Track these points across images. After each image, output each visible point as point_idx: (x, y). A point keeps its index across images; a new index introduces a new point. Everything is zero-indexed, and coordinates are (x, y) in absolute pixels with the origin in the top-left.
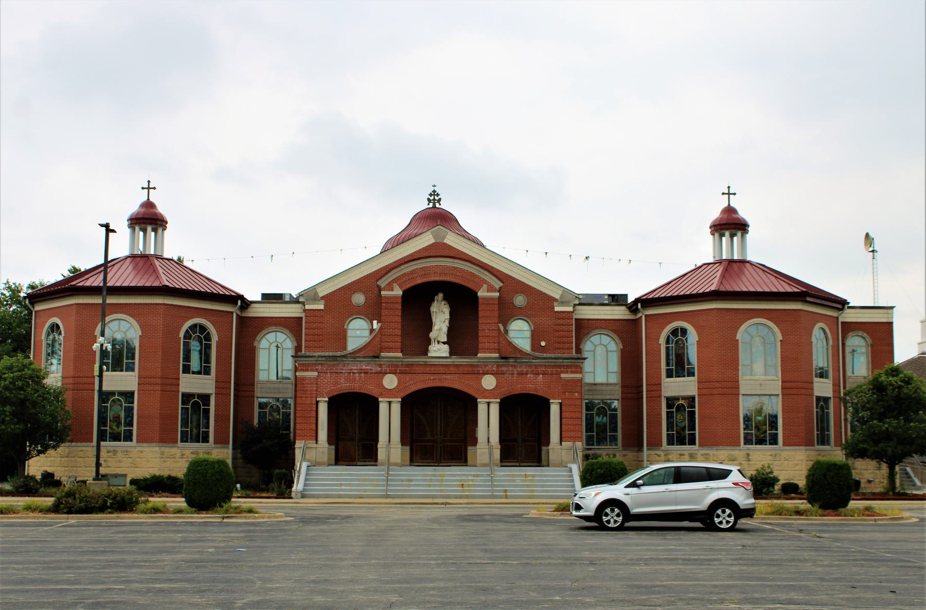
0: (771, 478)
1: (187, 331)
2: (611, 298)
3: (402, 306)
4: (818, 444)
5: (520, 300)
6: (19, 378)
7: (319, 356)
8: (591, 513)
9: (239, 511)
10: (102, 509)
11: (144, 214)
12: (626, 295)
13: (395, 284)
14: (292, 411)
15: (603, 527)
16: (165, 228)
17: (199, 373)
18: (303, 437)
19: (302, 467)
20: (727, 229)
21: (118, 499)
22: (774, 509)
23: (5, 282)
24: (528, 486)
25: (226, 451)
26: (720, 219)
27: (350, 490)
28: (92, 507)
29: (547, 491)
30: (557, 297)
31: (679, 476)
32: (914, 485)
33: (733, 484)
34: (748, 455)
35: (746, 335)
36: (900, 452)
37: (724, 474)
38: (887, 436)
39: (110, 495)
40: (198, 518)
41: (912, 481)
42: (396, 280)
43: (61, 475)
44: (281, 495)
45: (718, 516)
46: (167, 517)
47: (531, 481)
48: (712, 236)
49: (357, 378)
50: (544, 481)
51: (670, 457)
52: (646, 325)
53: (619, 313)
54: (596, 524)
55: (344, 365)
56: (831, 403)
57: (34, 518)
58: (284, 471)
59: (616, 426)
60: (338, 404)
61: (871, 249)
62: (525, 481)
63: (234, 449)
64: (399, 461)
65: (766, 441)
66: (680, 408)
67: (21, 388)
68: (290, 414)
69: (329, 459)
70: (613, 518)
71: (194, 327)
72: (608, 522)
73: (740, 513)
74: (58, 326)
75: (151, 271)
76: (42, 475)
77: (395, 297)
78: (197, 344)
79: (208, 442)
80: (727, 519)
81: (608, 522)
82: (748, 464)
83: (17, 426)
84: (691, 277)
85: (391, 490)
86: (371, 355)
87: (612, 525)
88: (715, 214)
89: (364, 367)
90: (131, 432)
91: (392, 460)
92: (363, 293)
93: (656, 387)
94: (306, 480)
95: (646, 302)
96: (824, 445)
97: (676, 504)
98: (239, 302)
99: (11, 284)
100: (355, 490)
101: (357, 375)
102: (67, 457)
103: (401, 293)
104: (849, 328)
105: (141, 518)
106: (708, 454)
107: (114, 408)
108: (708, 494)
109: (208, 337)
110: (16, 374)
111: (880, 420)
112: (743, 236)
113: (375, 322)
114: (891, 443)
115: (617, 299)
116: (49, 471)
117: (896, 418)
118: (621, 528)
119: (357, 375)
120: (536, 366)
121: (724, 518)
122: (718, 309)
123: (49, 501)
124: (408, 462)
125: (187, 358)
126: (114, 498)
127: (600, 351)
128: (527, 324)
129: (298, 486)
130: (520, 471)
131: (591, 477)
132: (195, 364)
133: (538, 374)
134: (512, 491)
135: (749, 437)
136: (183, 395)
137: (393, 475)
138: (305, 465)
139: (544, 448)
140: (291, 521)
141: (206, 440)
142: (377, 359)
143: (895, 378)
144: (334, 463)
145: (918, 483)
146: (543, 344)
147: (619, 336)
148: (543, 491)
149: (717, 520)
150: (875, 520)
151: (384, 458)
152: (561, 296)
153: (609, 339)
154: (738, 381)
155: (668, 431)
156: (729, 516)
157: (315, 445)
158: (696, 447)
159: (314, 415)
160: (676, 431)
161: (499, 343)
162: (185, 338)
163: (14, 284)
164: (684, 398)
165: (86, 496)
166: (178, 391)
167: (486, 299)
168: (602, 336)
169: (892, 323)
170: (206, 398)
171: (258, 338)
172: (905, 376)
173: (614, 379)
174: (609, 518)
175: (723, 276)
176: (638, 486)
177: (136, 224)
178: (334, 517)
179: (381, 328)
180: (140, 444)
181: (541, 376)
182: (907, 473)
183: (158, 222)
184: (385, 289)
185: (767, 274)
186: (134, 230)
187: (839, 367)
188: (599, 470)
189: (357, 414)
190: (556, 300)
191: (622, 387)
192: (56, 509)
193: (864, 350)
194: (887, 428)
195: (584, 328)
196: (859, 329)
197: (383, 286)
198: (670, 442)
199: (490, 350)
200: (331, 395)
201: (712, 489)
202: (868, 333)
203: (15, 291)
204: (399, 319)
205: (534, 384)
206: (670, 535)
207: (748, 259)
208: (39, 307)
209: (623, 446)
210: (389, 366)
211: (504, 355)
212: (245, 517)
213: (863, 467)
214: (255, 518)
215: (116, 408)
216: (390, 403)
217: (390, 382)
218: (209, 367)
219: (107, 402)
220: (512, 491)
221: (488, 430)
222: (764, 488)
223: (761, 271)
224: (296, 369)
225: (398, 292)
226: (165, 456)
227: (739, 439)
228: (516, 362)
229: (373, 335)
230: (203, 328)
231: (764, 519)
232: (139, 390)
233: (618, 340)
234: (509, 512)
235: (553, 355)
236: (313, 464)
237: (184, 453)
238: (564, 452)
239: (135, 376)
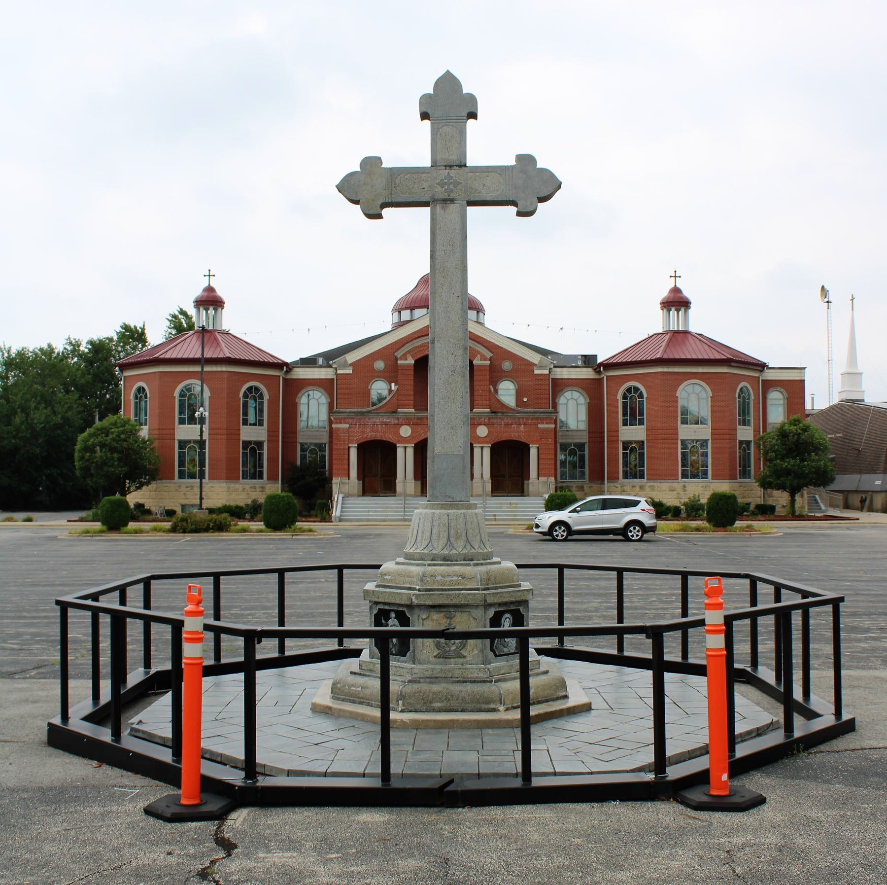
0: (698, 504)
1: (245, 392)
2: (583, 358)
3: (414, 377)
4: (740, 478)
5: (507, 365)
6: (123, 433)
7: (350, 412)
8: (546, 530)
9: (303, 531)
10: (207, 530)
11: (207, 297)
12: (596, 356)
14: (327, 453)
15: (554, 540)
16: (223, 308)
17: (255, 424)
18: (339, 475)
19: (337, 497)
20: (673, 306)
21: (217, 523)
22: (681, 527)
23: (67, 338)
24: (512, 512)
25: (276, 485)
26: (668, 297)
27: (376, 516)
28: (200, 529)
29: (527, 515)
30: (537, 362)
31: (606, 505)
32: (820, 509)
33: (642, 510)
34: (685, 486)
35: (684, 393)
36: (796, 484)
37: (635, 504)
38: (788, 472)
40: (275, 535)
41: (819, 506)
42: (408, 352)
43: (151, 505)
44: (323, 520)
45: (631, 531)
46: (253, 535)
47: (515, 507)
48: (661, 311)
49: (380, 429)
50: (524, 508)
51: (625, 488)
52: (607, 384)
53: (587, 373)
54: (550, 538)
55: (369, 419)
56: (752, 445)
57: (161, 536)
58: (324, 501)
59: (584, 464)
60: (365, 449)
61: (826, 300)
62: (510, 508)
63: (283, 483)
64: (413, 493)
65: (699, 476)
66: (633, 450)
67: (125, 440)
68: (325, 456)
69: (358, 491)
70: (560, 533)
71: (250, 389)
72: (557, 536)
73: (645, 529)
74: (144, 389)
75: (215, 344)
76: (134, 504)
77: (409, 365)
78: (253, 401)
79: (262, 479)
80: (637, 533)
81: (557, 536)
82: (685, 494)
83: (123, 469)
84: (644, 345)
85: (407, 516)
86: (390, 410)
87: (559, 538)
88: (664, 293)
89: (385, 420)
91: (408, 492)
92: (383, 360)
93: (614, 433)
94: (342, 508)
95: (608, 365)
96: (746, 478)
97: (603, 524)
98: (285, 368)
99: (72, 339)
100: (381, 516)
102: (155, 491)
103: (413, 362)
104: (768, 385)
105: (235, 536)
106: (653, 486)
107: (190, 453)
108: (625, 516)
109: (261, 396)
110: (121, 429)
111: (782, 459)
112: (685, 311)
113: (393, 385)
114: (790, 477)
115: (589, 360)
116: (140, 502)
117: (794, 458)
118: (565, 540)
120: (519, 419)
121: (635, 533)
122: (662, 372)
123: (168, 525)
124: (420, 494)
125: (246, 413)
126: (215, 522)
127: (571, 404)
128: (512, 384)
129: (336, 512)
130: (507, 500)
131: (553, 504)
132: (251, 418)
133: (520, 425)
134: (499, 515)
135: (685, 473)
136: (243, 442)
137: (408, 504)
138: (341, 496)
139: (526, 482)
140: (340, 537)
141: (261, 477)
143: (795, 427)
144: (361, 494)
145: (823, 507)
146: (525, 400)
147: (585, 391)
148: (524, 515)
149: (630, 534)
150: (750, 534)
151: (402, 491)
152: (540, 362)
153: (578, 394)
154: (677, 429)
155: (623, 468)
156: (638, 531)
157: (347, 481)
158: (645, 480)
159: (347, 458)
161: (490, 400)
162: (244, 396)
163: (74, 339)
164: (636, 442)
165: (195, 521)
167: (479, 366)
168: (573, 392)
169: (804, 380)
170: (260, 444)
171: (299, 396)
172: (804, 426)
173: (583, 426)
174: (558, 533)
175: (668, 345)
176: (578, 512)
177: (200, 305)
178: (370, 535)
179: (398, 390)
181: (523, 426)
182: (816, 500)
183: (218, 304)
184: (401, 359)
186: (199, 310)
187: (759, 416)
188: (557, 500)
189: (379, 456)
190: (536, 365)
191: (589, 433)
192: (174, 530)
193: (781, 402)
194: (786, 466)
195: (559, 386)
196: (778, 386)
197: (399, 356)
198: (626, 476)
199: (483, 407)
200: (359, 443)
201: (627, 513)
202: (785, 389)
203: (76, 345)
204: (412, 382)
205: (517, 433)
206: (595, 544)
207: (690, 330)
208: (128, 373)
209: (590, 479)
210: (404, 419)
211: (494, 410)
212: (308, 535)
213: (779, 495)
214: (314, 535)
215: (192, 453)
216: (405, 448)
217: (405, 431)
218: (262, 420)
220: (499, 515)
221: (482, 468)
222: (693, 512)
224: (331, 422)
225: (411, 361)
227: (678, 474)
228: (503, 415)
229: (391, 395)
230: (257, 389)
231: (672, 534)
232: (209, 439)
233: (586, 396)
234: (495, 531)
235: (532, 410)
236: (347, 496)
238: (540, 486)
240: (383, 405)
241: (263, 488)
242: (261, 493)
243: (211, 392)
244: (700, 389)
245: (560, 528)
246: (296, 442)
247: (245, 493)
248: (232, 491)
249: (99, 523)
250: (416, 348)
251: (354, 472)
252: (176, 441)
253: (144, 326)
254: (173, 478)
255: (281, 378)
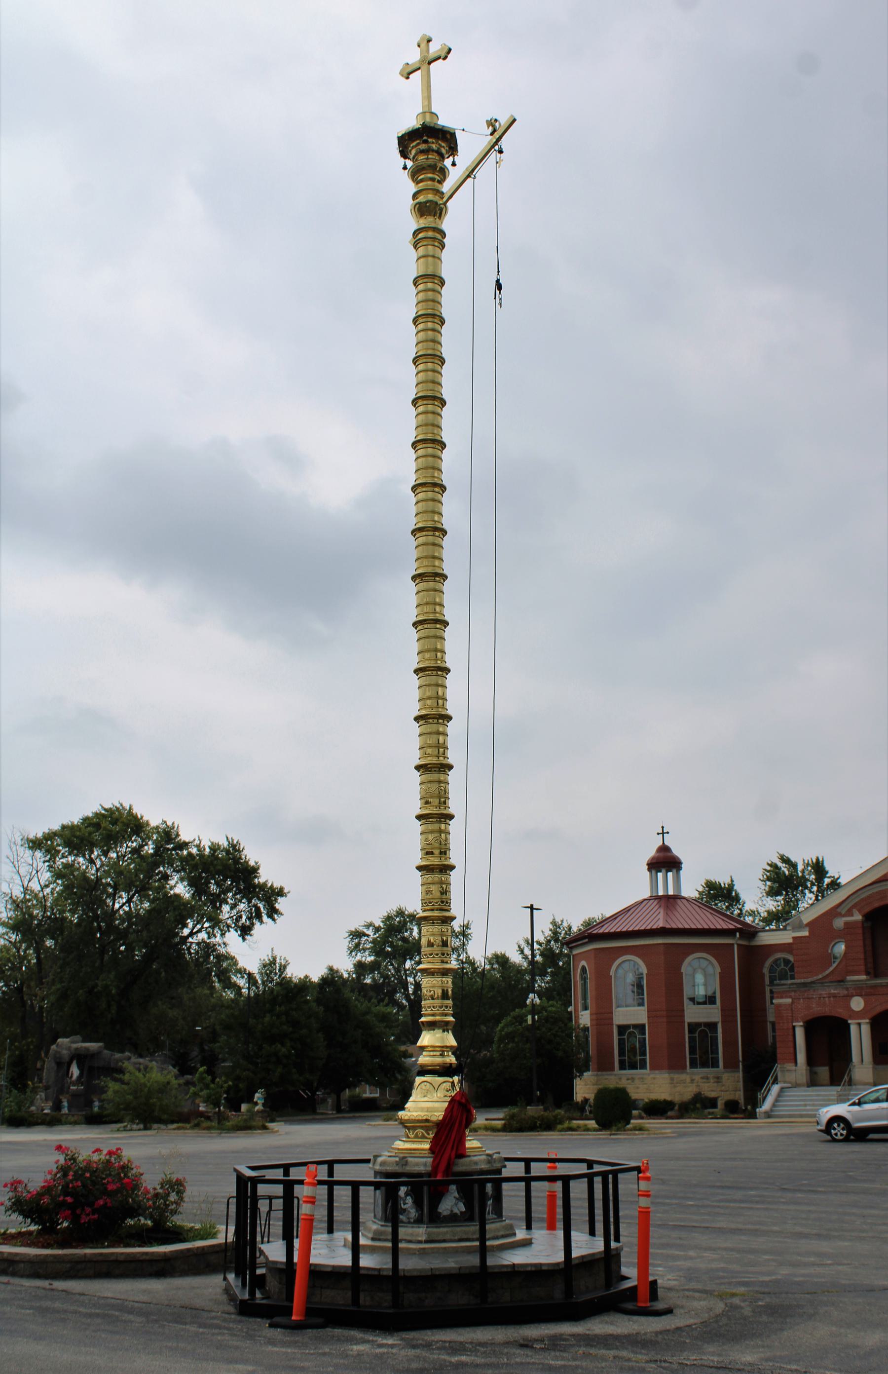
13: (854, 910)
25: (736, 1075)
39: (539, 1117)
42: (854, 906)
49: (827, 1002)
55: (814, 991)
60: (813, 1027)
77: (856, 922)
87: (839, 1137)
88: (651, 852)
89: (832, 991)
90: (644, 1061)
101: (827, 999)
107: (630, 1039)
118: (846, 1140)
119: (827, 999)
141: (715, 1064)
142: (842, 983)
157: (794, 1068)
158: (647, 1071)
160: (628, 1057)
166: (683, 1022)
170: (712, 1026)
180: (653, 1071)
185: (703, 910)
198: (622, 1067)
217: (857, 1004)
219: (695, 1033)
223: (697, 907)
225: (858, 917)
226: (675, 1081)
232: (648, 1023)
237: (694, 1078)
239: (718, 1009)
240: (830, 973)
241: (718, 1079)
242: (715, 1084)
243: (647, 969)
244: (620, 971)
245: (843, 1129)
246: (766, 1021)
247: (695, 1084)
248: (677, 1083)
249: (594, 1122)
250: (863, 900)
251: (801, 1057)
252: (615, 1026)
253: (732, 881)
254: (613, 1069)
255: (736, 946)
